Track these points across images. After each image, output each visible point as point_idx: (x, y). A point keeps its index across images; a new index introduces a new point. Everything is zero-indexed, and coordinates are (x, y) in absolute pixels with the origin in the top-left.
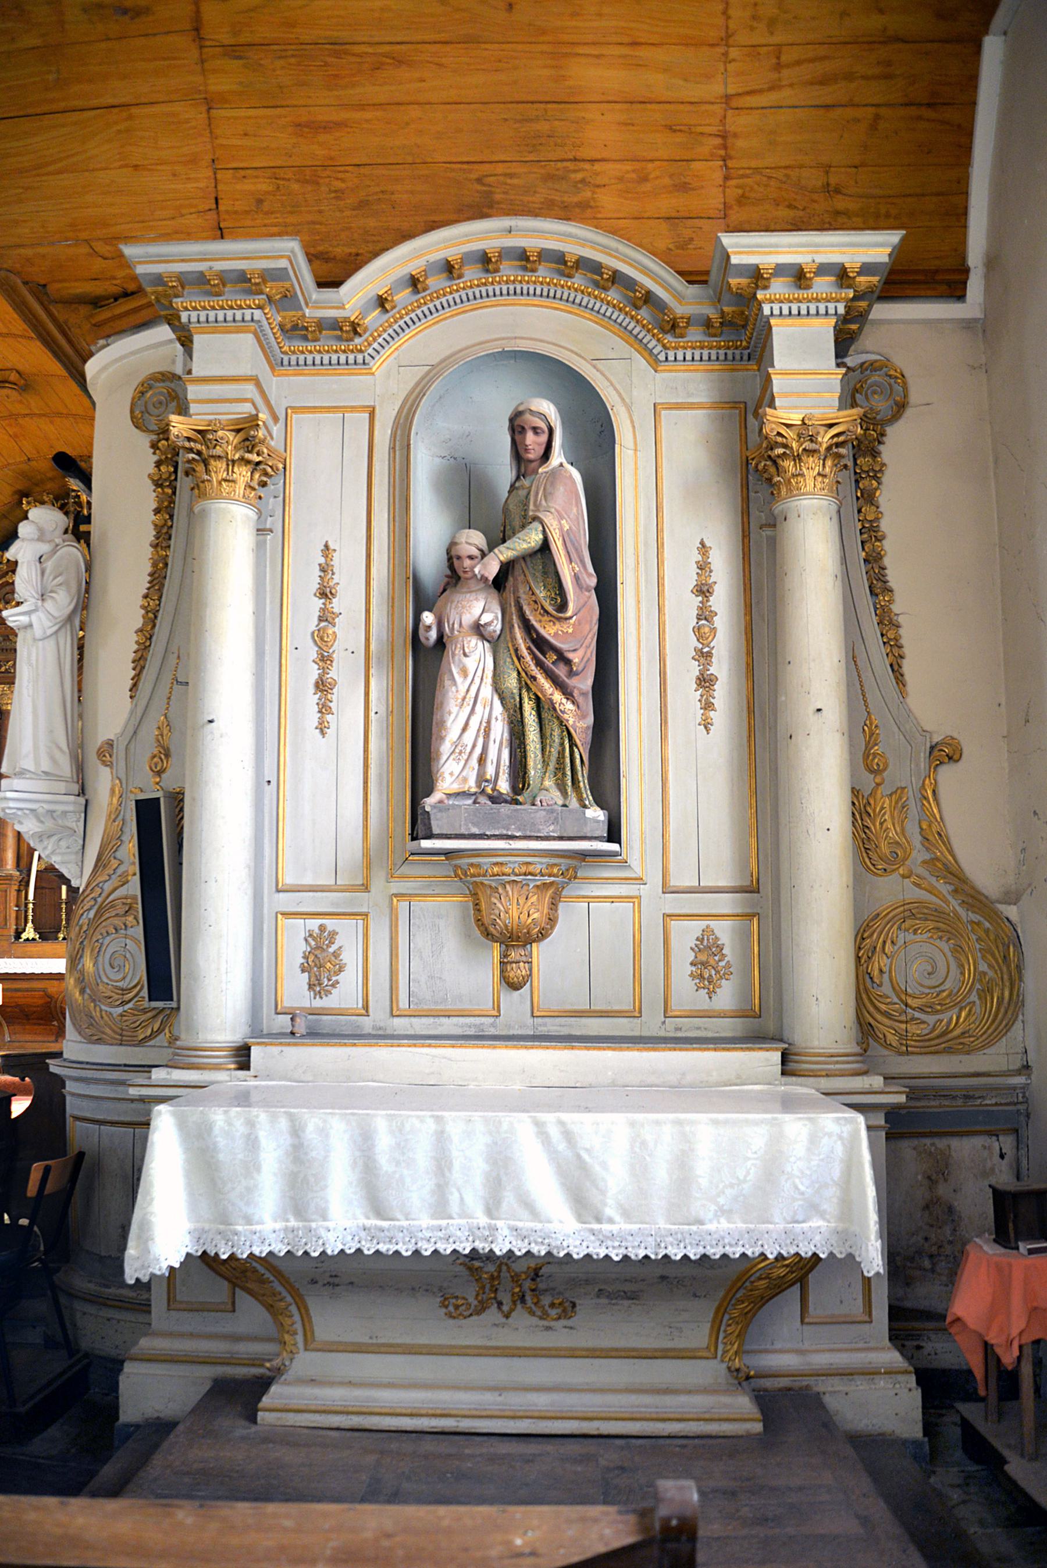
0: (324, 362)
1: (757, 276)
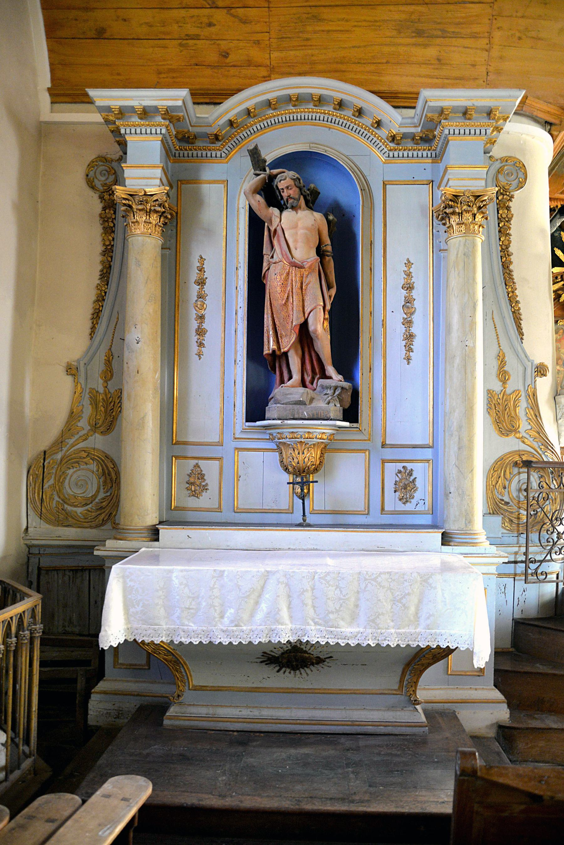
0: (189, 155)
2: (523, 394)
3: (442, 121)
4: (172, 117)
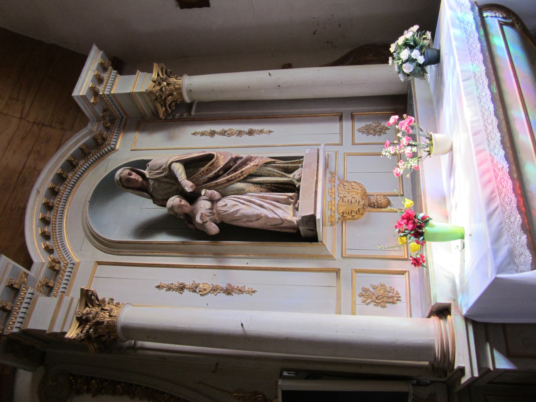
1: (94, 92)
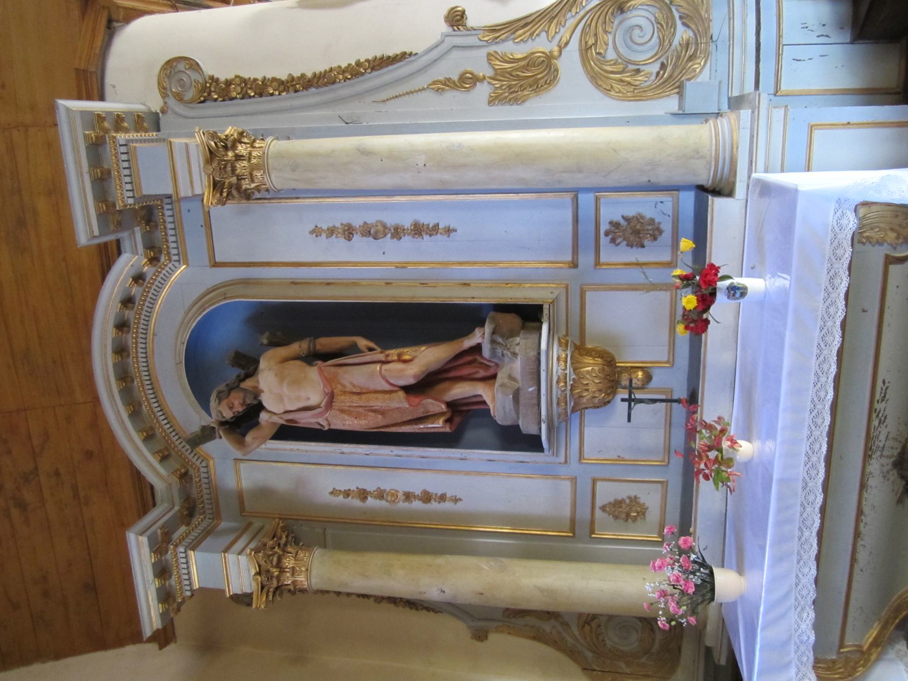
2: (492, 49)
3: (118, 209)
4: (163, 541)
